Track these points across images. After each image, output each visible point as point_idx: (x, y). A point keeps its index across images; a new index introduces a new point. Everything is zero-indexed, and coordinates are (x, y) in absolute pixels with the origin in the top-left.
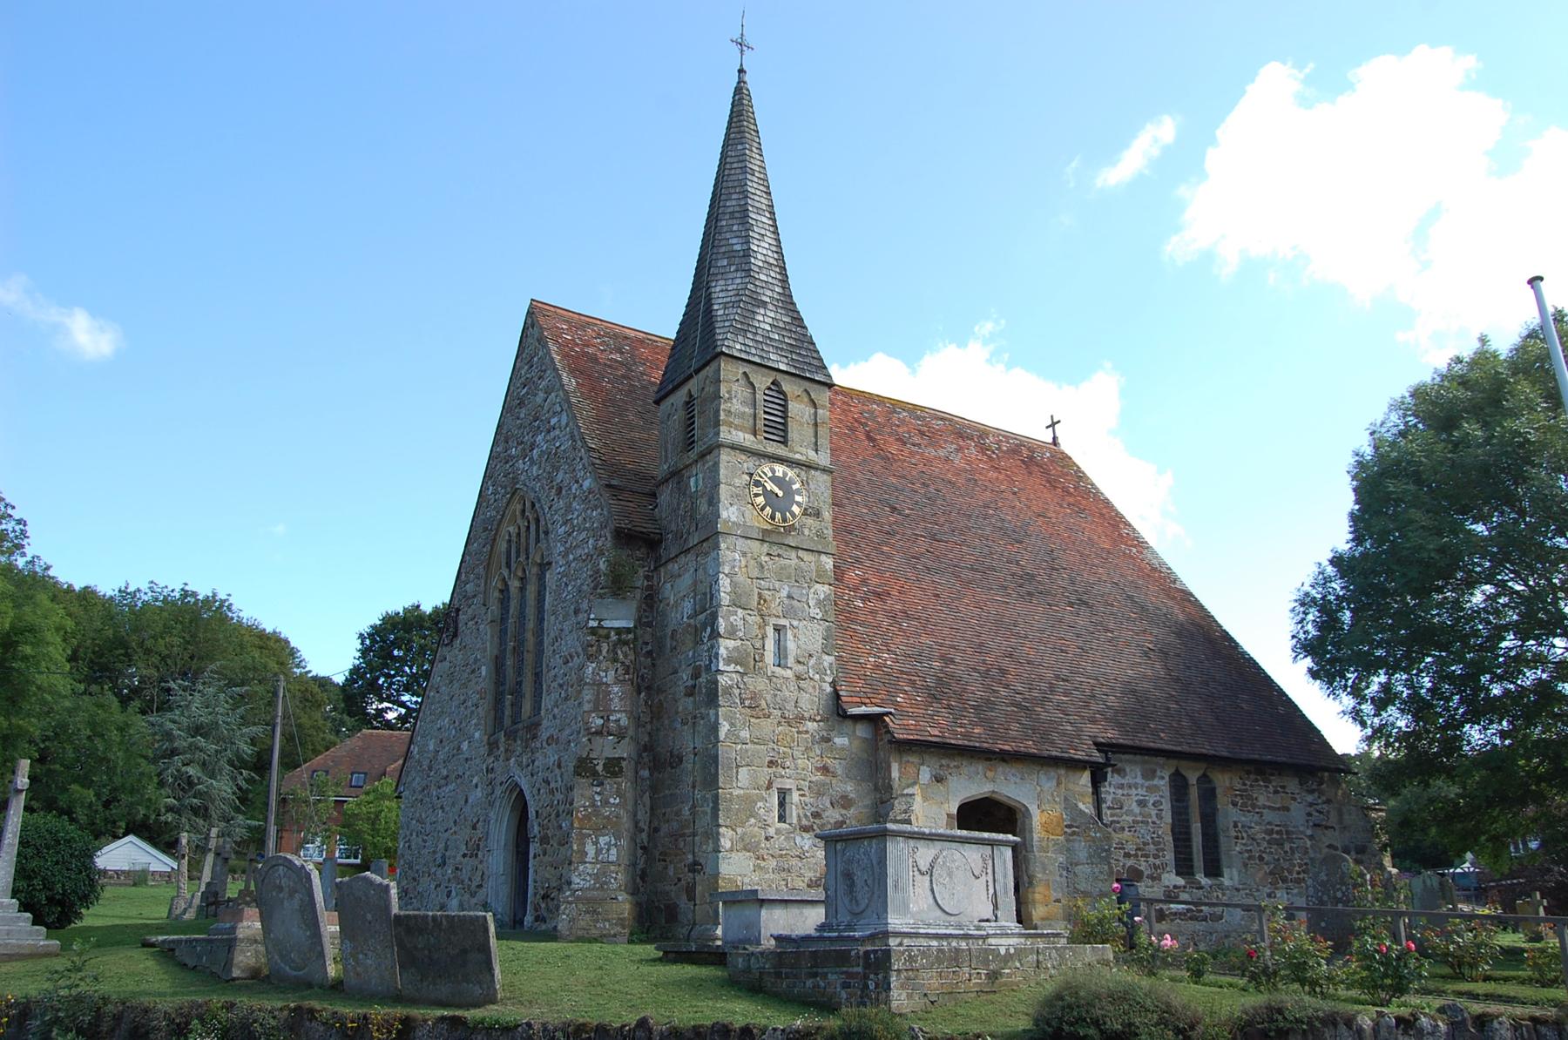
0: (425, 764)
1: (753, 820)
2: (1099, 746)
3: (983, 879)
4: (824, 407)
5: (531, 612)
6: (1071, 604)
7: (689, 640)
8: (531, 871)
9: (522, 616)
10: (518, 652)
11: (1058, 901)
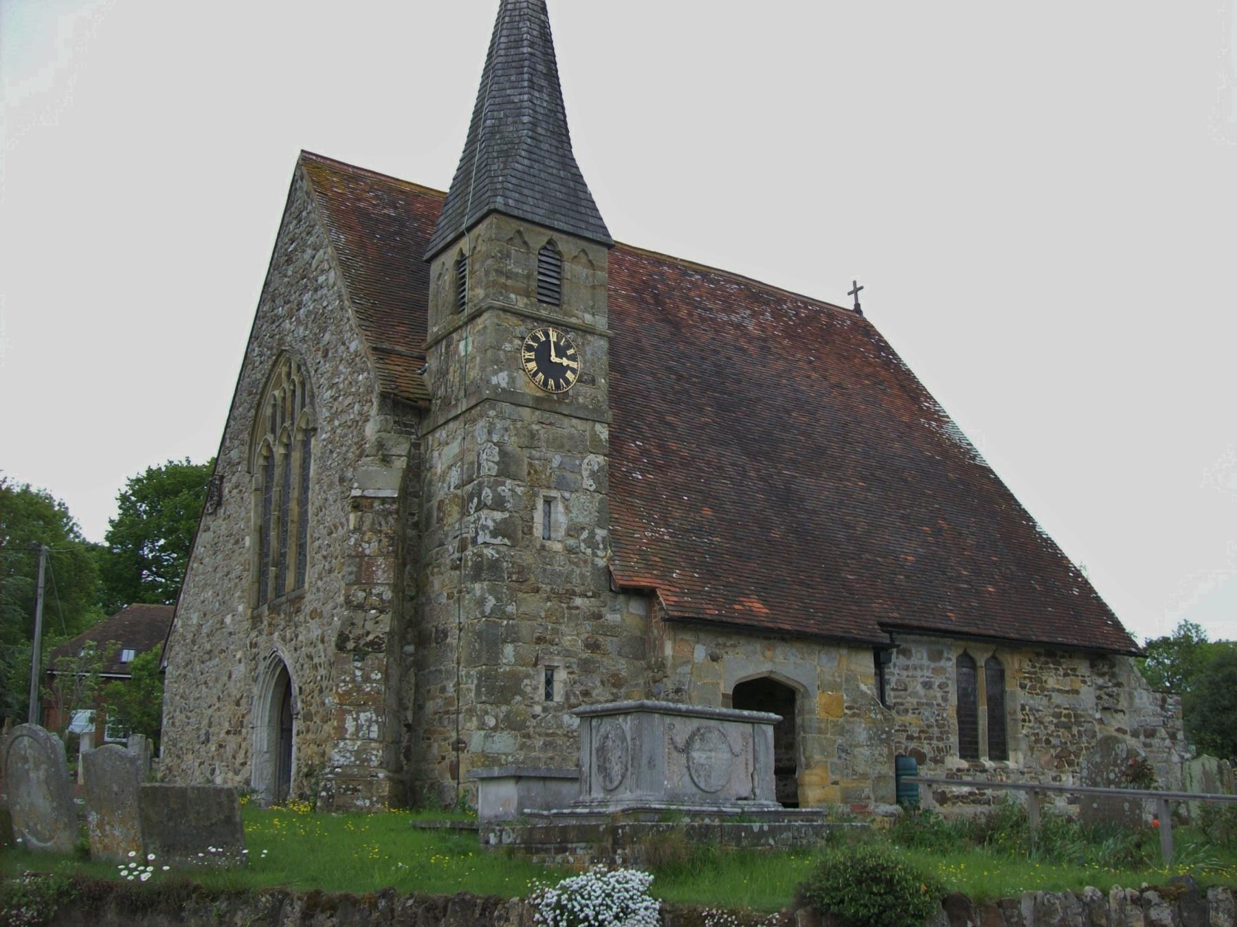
0: (190, 636)
1: (518, 698)
2: (882, 625)
3: (742, 759)
4: (602, 269)
5: (295, 479)
6: (863, 479)
7: (455, 511)
8: (294, 749)
9: (286, 485)
10: (282, 521)
11: (836, 783)
